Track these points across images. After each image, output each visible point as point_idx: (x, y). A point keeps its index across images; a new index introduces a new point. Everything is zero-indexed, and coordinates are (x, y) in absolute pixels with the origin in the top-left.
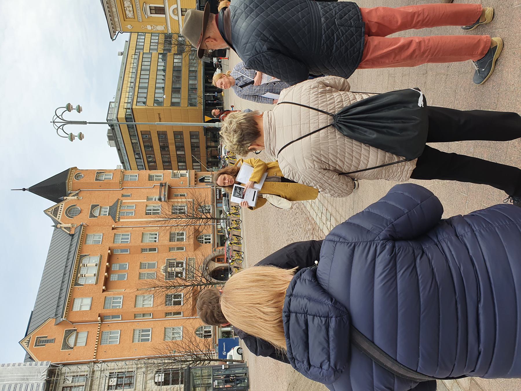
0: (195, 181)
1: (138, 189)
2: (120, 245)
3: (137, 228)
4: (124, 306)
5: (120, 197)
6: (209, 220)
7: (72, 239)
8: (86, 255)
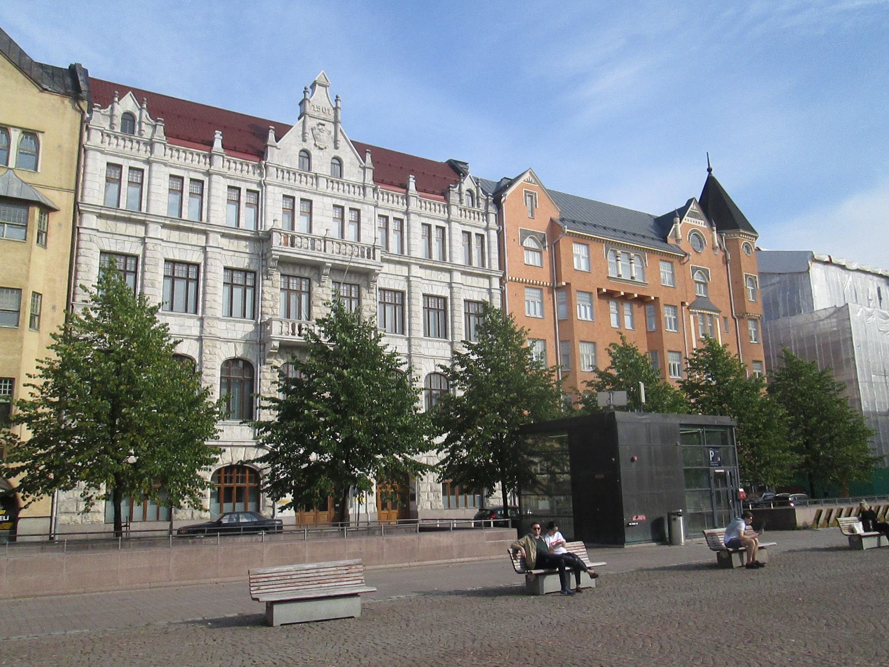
5: (723, 314)
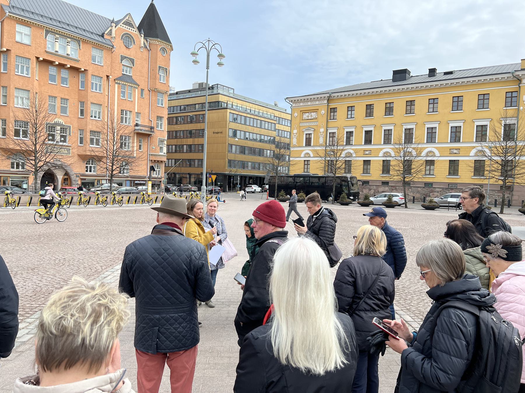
0: (155, 161)
1: (148, 105)
2: (89, 82)
3: (107, 100)
4: (18, 76)
5: (141, 87)
6: (111, 172)
7: (99, 35)
8: (80, 46)
